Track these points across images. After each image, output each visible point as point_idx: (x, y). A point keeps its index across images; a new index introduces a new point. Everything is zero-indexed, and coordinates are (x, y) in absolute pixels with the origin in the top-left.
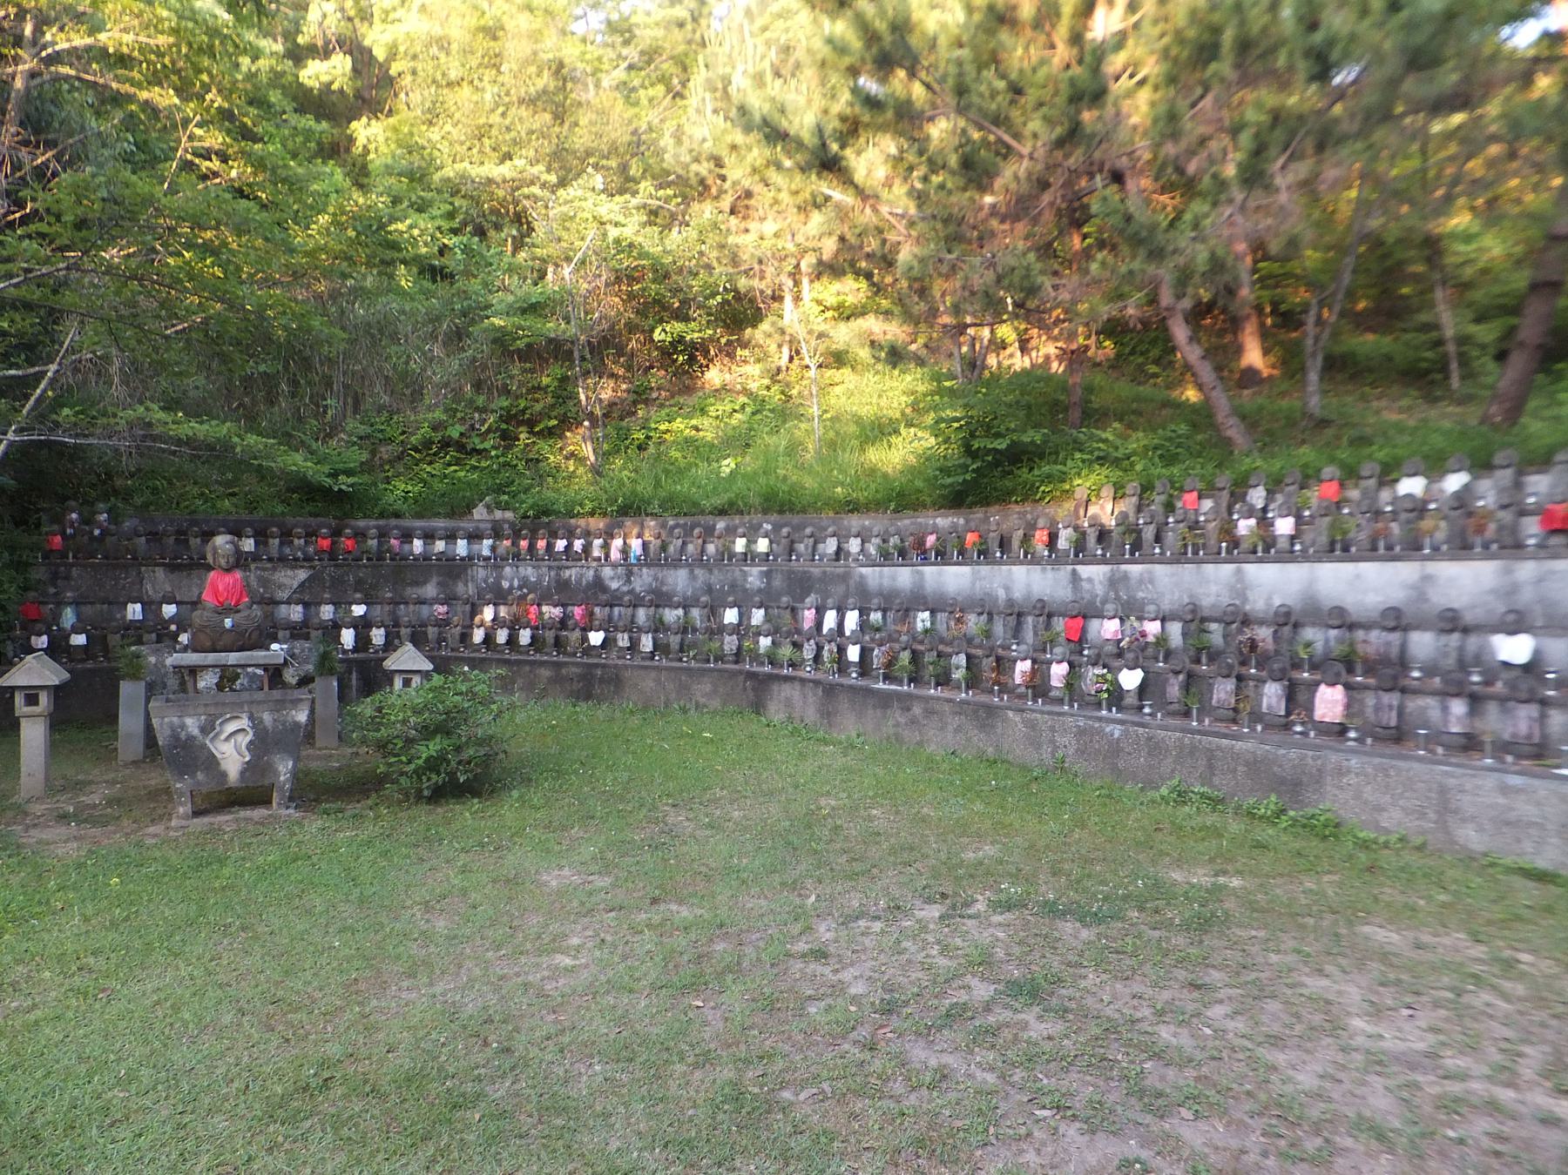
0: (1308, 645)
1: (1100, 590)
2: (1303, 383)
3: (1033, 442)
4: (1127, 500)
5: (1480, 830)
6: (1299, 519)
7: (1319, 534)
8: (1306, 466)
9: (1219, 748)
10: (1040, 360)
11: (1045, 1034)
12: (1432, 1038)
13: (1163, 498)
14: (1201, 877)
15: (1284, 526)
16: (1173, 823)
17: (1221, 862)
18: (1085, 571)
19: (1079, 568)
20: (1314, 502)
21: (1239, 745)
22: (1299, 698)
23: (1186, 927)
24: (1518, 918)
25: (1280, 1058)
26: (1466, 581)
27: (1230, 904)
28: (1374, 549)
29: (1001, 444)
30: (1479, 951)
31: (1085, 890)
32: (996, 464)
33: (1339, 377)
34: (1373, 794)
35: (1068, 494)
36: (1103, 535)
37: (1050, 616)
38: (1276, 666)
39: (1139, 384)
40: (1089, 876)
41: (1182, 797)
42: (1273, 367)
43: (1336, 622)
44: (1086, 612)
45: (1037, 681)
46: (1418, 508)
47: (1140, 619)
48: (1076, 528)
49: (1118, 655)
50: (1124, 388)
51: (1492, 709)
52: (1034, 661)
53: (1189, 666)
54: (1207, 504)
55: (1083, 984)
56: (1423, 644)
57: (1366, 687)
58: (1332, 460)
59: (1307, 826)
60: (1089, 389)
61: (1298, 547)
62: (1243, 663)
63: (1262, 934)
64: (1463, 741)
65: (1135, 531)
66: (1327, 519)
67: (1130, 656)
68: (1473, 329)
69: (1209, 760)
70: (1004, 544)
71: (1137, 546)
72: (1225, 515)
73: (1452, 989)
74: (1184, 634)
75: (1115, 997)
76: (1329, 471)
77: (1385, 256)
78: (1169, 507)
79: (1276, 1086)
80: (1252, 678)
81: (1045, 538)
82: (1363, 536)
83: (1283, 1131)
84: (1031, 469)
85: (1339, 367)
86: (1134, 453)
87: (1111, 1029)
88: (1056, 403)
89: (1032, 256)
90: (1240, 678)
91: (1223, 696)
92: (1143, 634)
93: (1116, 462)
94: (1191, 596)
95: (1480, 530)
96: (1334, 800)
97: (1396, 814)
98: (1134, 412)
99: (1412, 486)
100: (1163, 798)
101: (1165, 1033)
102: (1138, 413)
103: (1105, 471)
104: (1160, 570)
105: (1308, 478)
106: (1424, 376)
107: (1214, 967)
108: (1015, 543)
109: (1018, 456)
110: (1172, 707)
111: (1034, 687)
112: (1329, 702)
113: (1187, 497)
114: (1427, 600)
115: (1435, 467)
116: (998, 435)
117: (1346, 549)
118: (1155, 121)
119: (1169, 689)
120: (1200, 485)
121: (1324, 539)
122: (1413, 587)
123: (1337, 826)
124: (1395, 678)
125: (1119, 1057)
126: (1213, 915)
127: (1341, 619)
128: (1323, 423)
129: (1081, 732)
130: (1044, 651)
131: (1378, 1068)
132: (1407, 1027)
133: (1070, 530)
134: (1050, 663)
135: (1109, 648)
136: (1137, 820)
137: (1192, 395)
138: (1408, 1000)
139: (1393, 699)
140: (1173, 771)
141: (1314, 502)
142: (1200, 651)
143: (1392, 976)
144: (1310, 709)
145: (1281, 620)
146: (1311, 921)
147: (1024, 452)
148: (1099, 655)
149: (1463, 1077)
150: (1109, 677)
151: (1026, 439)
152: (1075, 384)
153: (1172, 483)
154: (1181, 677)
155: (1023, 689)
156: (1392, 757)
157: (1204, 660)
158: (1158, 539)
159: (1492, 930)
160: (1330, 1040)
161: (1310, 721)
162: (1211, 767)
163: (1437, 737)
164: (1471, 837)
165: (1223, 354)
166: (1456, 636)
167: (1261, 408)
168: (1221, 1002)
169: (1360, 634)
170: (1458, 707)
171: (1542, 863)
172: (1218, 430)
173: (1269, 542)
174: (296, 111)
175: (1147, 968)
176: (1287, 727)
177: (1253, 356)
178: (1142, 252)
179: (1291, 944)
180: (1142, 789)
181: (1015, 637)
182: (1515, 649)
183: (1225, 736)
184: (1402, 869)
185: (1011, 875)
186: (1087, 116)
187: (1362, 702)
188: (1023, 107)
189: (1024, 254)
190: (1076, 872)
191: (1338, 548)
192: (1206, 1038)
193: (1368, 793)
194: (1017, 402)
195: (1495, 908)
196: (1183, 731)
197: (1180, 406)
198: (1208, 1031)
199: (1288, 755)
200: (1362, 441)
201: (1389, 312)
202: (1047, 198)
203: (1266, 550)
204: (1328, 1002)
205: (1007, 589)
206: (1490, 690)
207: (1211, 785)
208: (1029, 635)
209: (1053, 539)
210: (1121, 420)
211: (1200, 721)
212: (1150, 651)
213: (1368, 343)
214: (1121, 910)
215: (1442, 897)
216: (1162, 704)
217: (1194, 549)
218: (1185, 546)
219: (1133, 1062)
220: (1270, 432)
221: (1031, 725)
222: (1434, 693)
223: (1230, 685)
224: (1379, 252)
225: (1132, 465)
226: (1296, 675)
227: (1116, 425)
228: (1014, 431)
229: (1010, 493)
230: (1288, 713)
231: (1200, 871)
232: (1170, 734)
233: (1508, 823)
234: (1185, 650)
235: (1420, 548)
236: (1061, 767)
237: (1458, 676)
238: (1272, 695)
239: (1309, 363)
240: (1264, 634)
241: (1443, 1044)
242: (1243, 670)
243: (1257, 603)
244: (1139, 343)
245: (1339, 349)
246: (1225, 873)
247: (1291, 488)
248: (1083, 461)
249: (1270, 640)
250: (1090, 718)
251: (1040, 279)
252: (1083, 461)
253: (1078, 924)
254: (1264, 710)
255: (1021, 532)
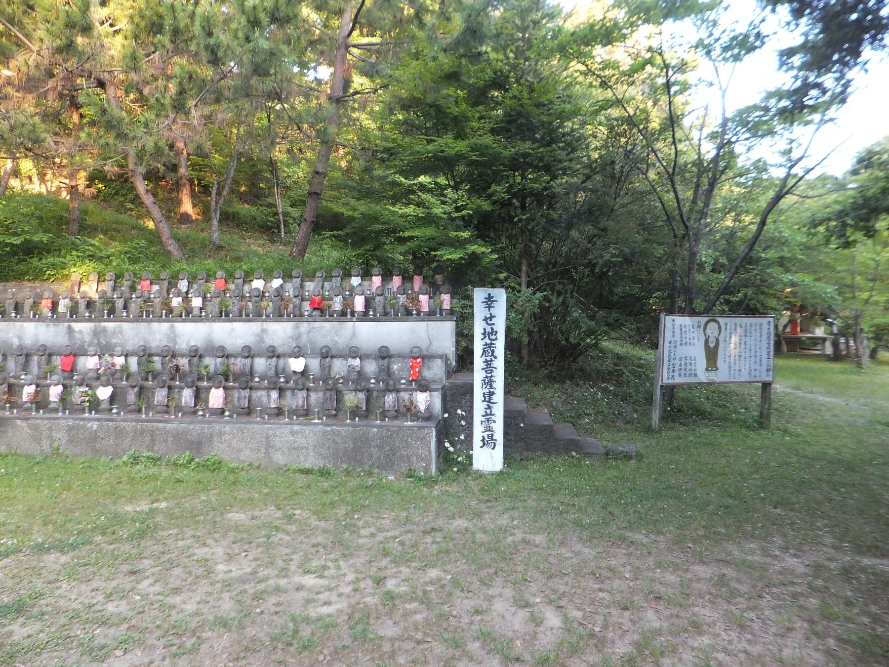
0: (206, 367)
1: (87, 338)
2: (211, 226)
3: (41, 242)
4: (107, 283)
5: (283, 454)
6: (205, 299)
7: (213, 307)
8: (209, 270)
9: (157, 428)
10: (54, 189)
11: (25, 635)
12: (254, 564)
13: (129, 283)
14: (144, 506)
15: (197, 302)
16: (129, 477)
17: (155, 496)
18: (77, 326)
19: (73, 325)
20: (212, 289)
21: (169, 426)
22: (200, 396)
23: (131, 538)
24: (297, 494)
25: (178, 599)
26: (280, 332)
27: (159, 519)
28: (241, 316)
29: (17, 241)
30: (279, 514)
31: (66, 531)
32: (13, 253)
33: (231, 225)
34: (235, 442)
35: (67, 277)
36: (90, 304)
37: (50, 355)
38: (189, 380)
39: (121, 213)
40: (70, 520)
41: (136, 460)
42: (199, 215)
43: (221, 355)
44: (75, 353)
45: (39, 399)
46: (261, 295)
47: (112, 355)
48: (72, 299)
49: (98, 378)
50: (109, 214)
51: (289, 394)
52: (37, 386)
53: (141, 382)
54: (156, 288)
55: (58, 592)
56: (261, 364)
57: (234, 388)
58: (222, 268)
59: (204, 466)
60: (86, 212)
61: (203, 314)
62: (173, 379)
63: (175, 531)
64: (276, 411)
65: (110, 303)
66: (218, 299)
67: (103, 379)
68: (290, 209)
69: (152, 436)
70: (18, 308)
71: (112, 311)
72: (165, 294)
73: (265, 536)
74: (139, 364)
75: (80, 594)
76: (220, 274)
77: (254, 165)
78: (133, 289)
79: (175, 616)
80: (176, 387)
81: (50, 305)
82: (235, 309)
83: (176, 641)
84: (41, 259)
85: (228, 218)
86: (113, 255)
87: (75, 616)
88: (61, 218)
89: (37, 119)
90: (170, 388)
91: (160, 398)
92: (113, 365)
93: (100, 259)
94: (145, 342)
95: (286, 308)
96: (219, 450)
97: (247, 452)
98: (115, 230)
99: (258, 284)
100: (124, 463)
101: (111, 608)
102: (117, 231)
103: (92, 264)
104: (125, 326)
105: (209, 276)
106: (269, 229)
107: (145, 558)
108: (27, 308)
109: (29, 250)
110: (130, 408)
111: (37, 403)
112: (216, 397)
113: (143, 283)
114: (264, 342)
115: (268, 276)
116: (15, 234)
117: (227, 315)
118: (124, 57)
119: (128, 397)
120: (153, 277)
121: (217, 310)
122: (258, 335)
123: (220, 463)
124: (247, 382)
125: (79, 633)
126: (148, 527)
127: (225, 354)
128: (220, 248)
129: (71, 429)
130: (46, 378)
131: (228, 588)
132: (244, 562)
133: (67, 300)
134: (49, 386)
135: (91, 374)
136: (107, 479)
137: (151, 225)
138: (245, 547)
139: (246, 393)
140: (131, 446)
141: (212, 289)
142: (148, 373)
143: (239, 537)
144: (207, 402)
145: (193, 354)
146: (202, 517)
147: (35, 247)
148: (83, 379)
149: (265, 579)
150: (90, 392)
151: (36, 238)
152: (74, 208)
153: (135, 275)
154: (136, 389)
155: (29, 405)
156: (245, 423)
157: (150, 378)
158: (125, 307)
159: (285, 502)
160: (206, 581)
161: (206, 408)
162: (153, 440)
163: (265, 411)
164: (279, 458)
165: (170, 206)
166: (274, 359)
167: (188, 237)
168: (148, 577)
169: (232, 360)
170: (274, 395)
171: (307, 465)
172: (164, 246)
173: (189, 311)
174: (209, 62)
175: (104, 571)
176: (195, 413)
177: (187, 207)
178: (113, 134)
179: (190, 533)
180: (111, 459)
181: (24, 370)
182: (297, 365)
183: (161, 422)
184: (249, 480)
185: (11, 532)
186: (79, 40)
187: (232, 396)
188: (34, 19)
189: (32, 116)
190: (60, 520)
191: (224, 315)
192: (136, 602)
193: (234, 444)
194: (32, 214)
195: (287, 491)
196: (137, 421)
197: (144, 229)
198: (138, 598)
199: (194, 428)
200: (238, 259)
201: (255, 196)
202: (51, 83)
203: (187, 315)
204: (207, 560)
205: (20, 338)
206: (288, 385)
207: (153, 451)
208: (34, 369)
209: (54, 306)
210: (105, 234)
211: (147, 414)
212: (118, 375)
213: (245, 209)
214: (90, 537)
215: (266, 491)
216: (124, 406)
217: (147, 314)
218: (142, 312)
219: (87, 633)
220: (192, 249)
221: (35, 428)
222: (265, 389)
223: (164, 392)
224: (250, 163)
225: (111, 261)
226: (199, 384)
227: (101, 236)
228: (27, 232)
229: (24, 274)
230: (196, 405)
231: (143, 503)
232: (128, 423)
233: (294, 449)
234: (139, 373)
235: (261, 316)
236: (56, 452)
237: (274, 379)
238: (187, 396)
239: (213, 215)
240: (183, 362)
241: (259, 565)
242: (172, 383)
243: (182, 345)
244: (115, 187)
245: (230, 210)
246: (157, 501)
247: (201, 281)
248: (78, 257)
249: (187, 365)
250: (77, 419)
251: (43, 135)
252: (78, 257)
253: (59, 554)
254: (183, 404)
255: (31, 300)
